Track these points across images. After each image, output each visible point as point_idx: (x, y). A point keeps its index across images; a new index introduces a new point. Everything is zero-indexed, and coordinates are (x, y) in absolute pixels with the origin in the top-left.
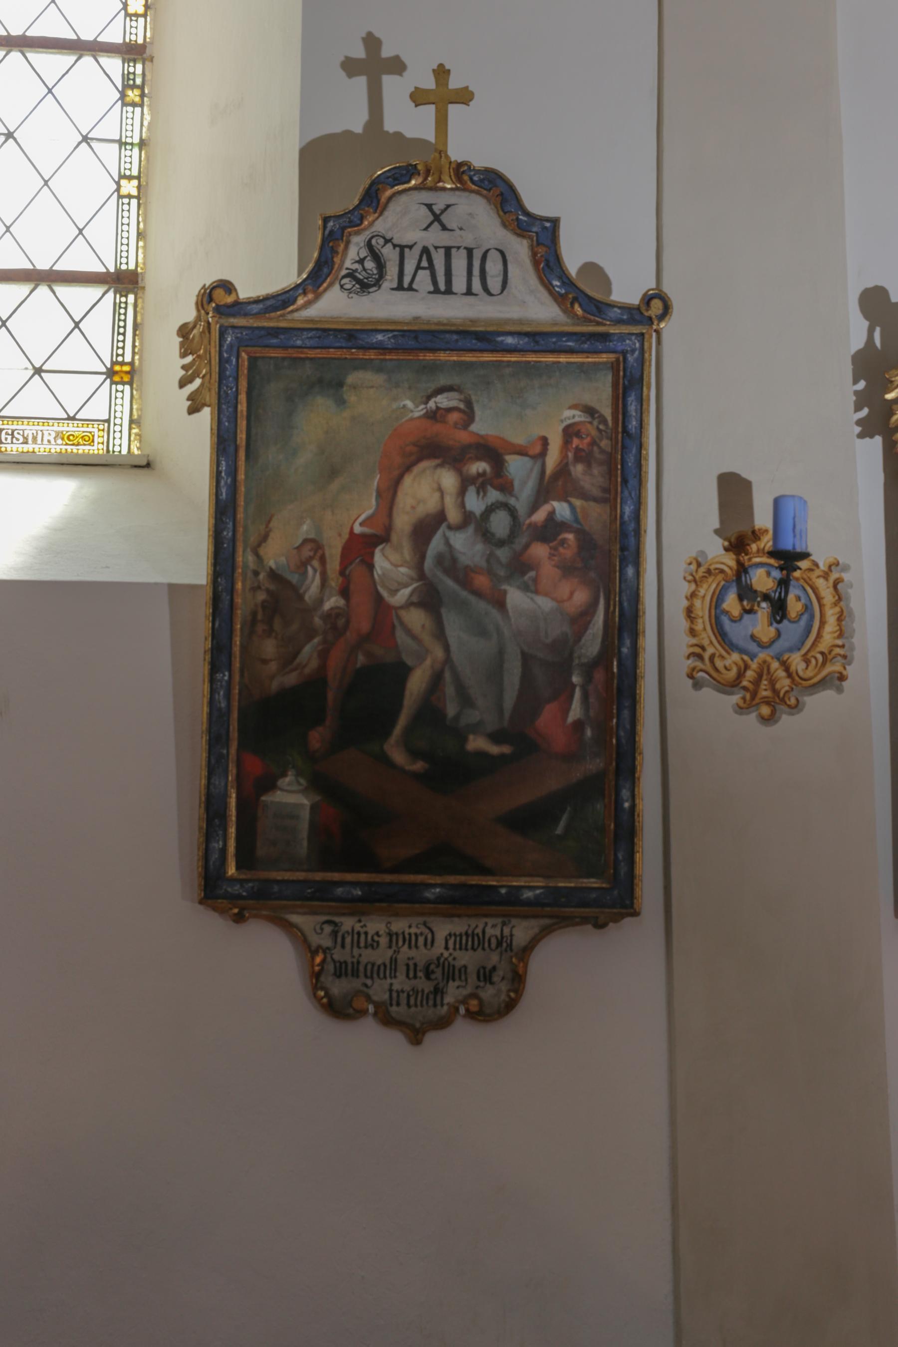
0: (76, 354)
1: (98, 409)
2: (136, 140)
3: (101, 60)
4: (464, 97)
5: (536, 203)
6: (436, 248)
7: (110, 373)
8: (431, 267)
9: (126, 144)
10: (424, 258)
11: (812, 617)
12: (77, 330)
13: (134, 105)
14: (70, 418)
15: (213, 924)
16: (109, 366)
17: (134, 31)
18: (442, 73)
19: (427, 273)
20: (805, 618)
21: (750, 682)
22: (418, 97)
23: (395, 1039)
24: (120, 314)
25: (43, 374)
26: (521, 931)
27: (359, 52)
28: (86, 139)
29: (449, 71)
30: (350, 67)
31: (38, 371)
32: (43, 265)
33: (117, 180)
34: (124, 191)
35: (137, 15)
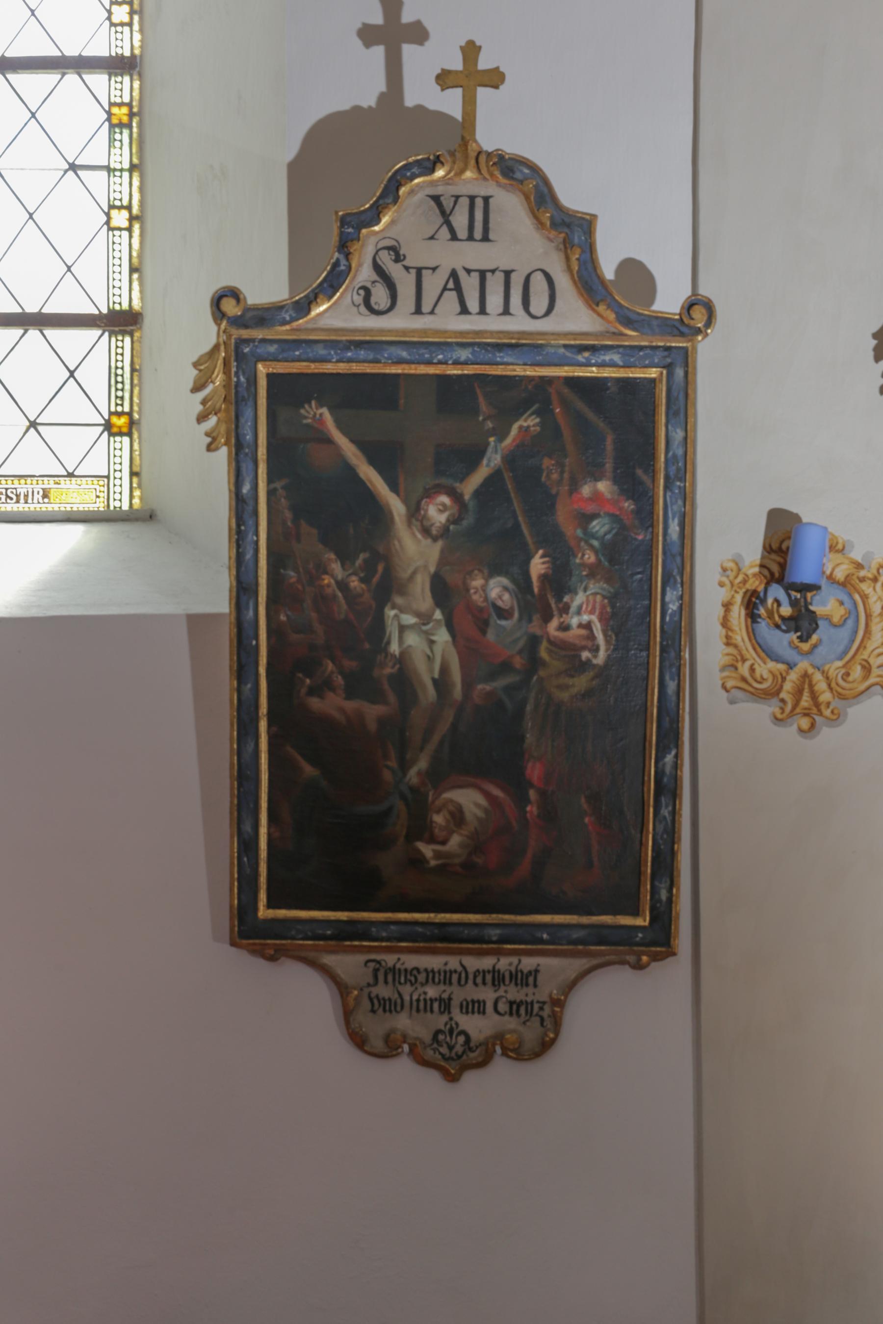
0: (72, 406)
1: (97, 464)
2: (126, 166)
3: (46, 332)
4: (495, 79)
5: (571, 196)
6: (469, 271)
7: (108, 426)
8: (458, 288)
9: (115, 170)
10: (451, 281)
11: (857, 620)
12: (72, 379)
13: (121, 125)
14: (71, 475)
15: (244, 966)
16: (107, 417)
17: (119, 43)
18: (471, 50)
19: (454, 294)
20: (850, 623)
21: (789, 693)
22: (444, 79)
23: (434, 1076)
24: (116, 375)
25: (40, 428)
26: (553, 968)
27: (457, 64)
28: (33, 425)
29: (480, 47)
30: (368, 35)
31: (33, 425)
32: (32, 308)
33: (106, 210)
34: (115, 19)
35: (122, 24)
